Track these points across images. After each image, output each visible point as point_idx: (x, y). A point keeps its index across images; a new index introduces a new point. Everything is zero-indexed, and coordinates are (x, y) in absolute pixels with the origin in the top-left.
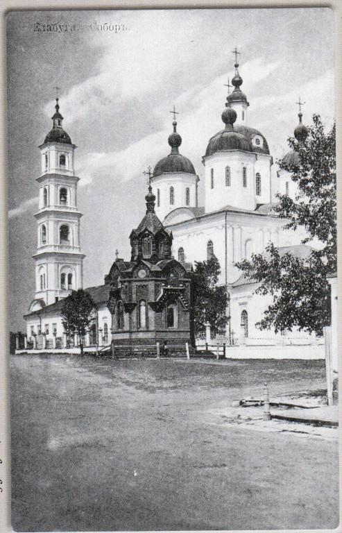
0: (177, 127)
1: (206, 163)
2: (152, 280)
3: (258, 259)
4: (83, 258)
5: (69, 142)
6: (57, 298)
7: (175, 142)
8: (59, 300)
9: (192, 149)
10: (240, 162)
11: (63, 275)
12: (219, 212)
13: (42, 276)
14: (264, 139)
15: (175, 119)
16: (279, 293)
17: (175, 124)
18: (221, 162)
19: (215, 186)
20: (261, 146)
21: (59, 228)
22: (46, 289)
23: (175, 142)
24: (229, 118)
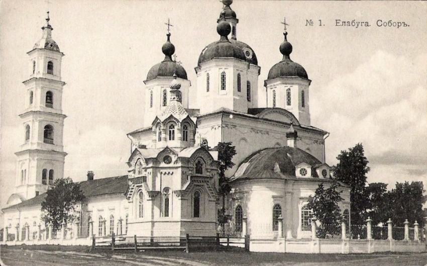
0: (170, 37)
1: (204, 66)
2: (292, 180)
3: (339, 155)
4: (65, 155)
5: (58, 51)
6: (37, 193)
7: (169, 51)
8: (40, 194)
9: (186, 58)
10: (218, 68)
11: (44, 172)
12: (218, 113)
13: (22, 171)
14: (253, 51)
15: (285, 29)
16: (367, 185)
17: (286, 34)
18: (214, 69)
19: (210, 90)
20: (250, 57)
21: (43, 127)
22: (27, 183)
23: (169, 51)
24: (224, 31)
